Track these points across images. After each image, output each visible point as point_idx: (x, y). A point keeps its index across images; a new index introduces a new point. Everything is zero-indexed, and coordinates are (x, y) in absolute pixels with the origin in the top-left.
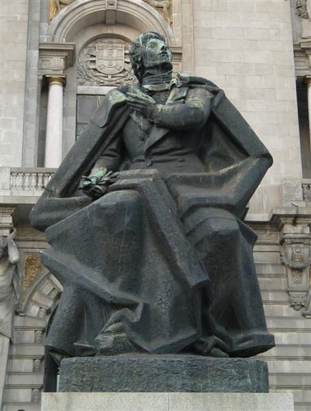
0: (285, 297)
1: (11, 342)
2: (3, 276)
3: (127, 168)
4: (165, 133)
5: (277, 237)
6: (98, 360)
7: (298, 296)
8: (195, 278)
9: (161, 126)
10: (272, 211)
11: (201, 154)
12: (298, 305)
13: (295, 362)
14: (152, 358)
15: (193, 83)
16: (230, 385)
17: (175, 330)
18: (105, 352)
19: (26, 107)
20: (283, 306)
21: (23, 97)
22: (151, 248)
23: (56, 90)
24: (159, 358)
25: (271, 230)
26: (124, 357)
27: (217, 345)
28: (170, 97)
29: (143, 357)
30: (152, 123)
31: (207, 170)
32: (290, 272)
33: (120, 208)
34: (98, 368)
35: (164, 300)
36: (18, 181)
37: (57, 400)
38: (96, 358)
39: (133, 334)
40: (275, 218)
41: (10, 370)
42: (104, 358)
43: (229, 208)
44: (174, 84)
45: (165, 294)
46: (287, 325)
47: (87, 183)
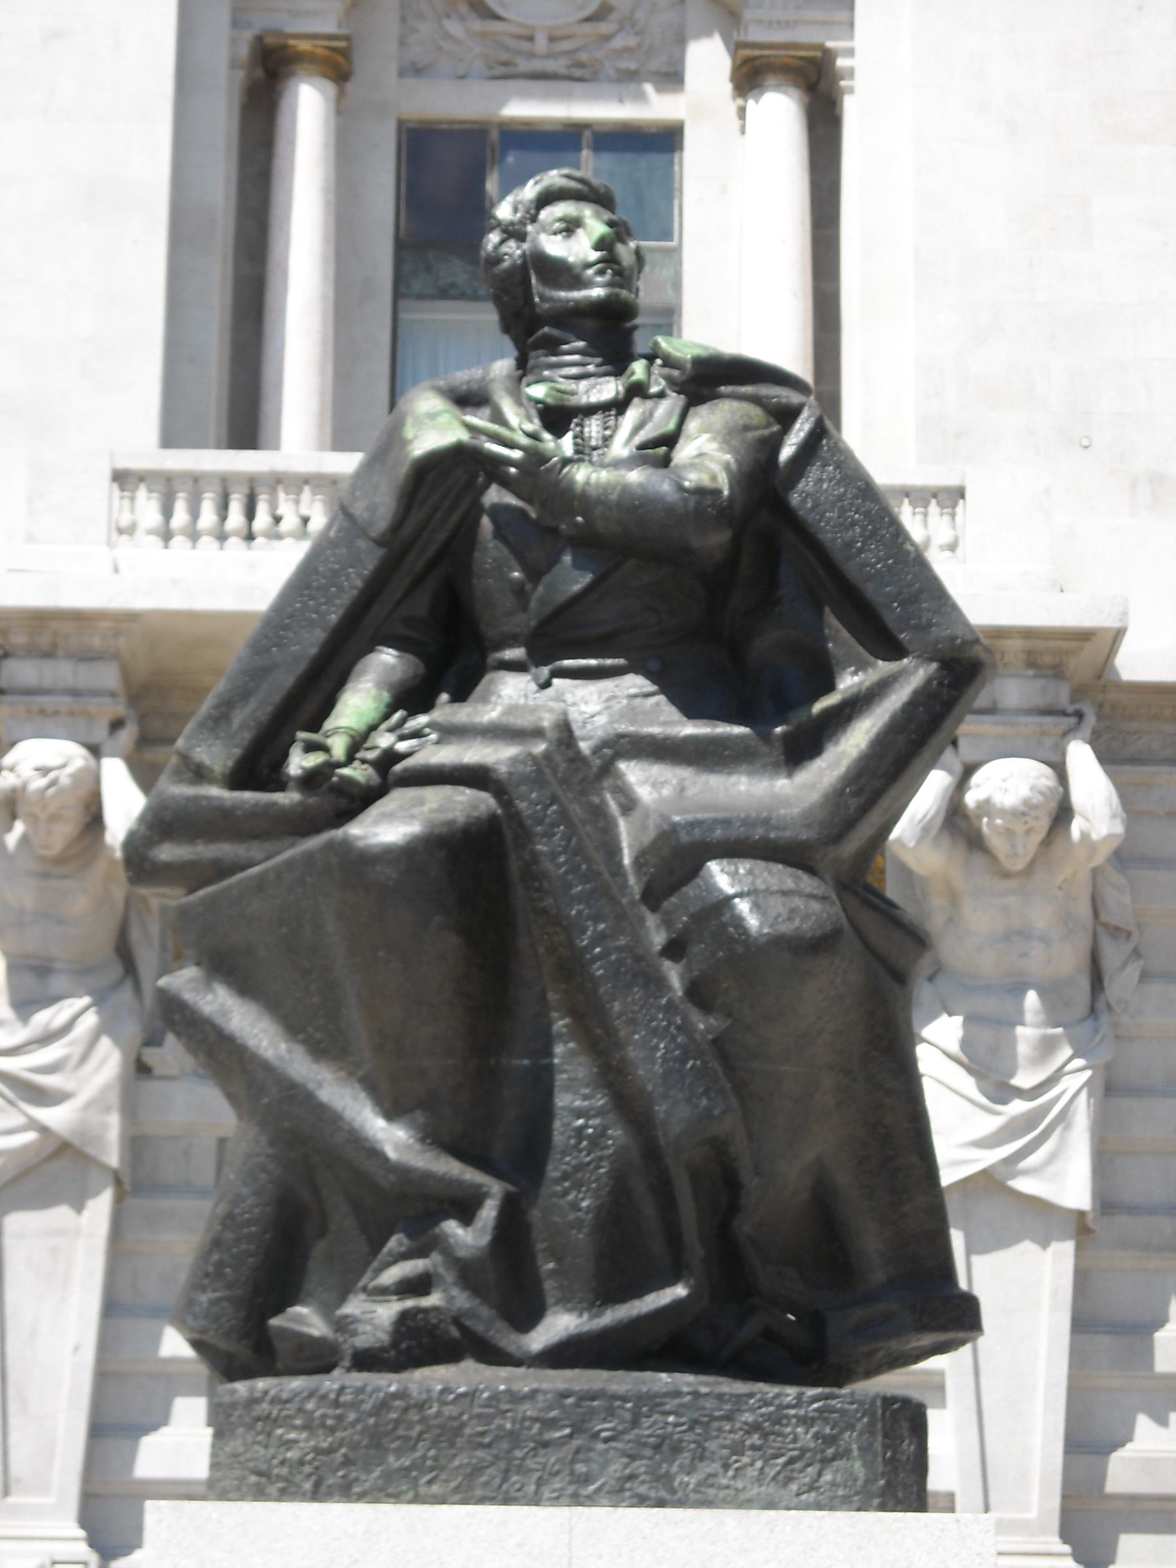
14: (523, 1379)
15: (708, 379)
18: (366, 1361)
23: (309, 106)
38: (329, 1383)
42: (358, 1378)
47: (314, 760)
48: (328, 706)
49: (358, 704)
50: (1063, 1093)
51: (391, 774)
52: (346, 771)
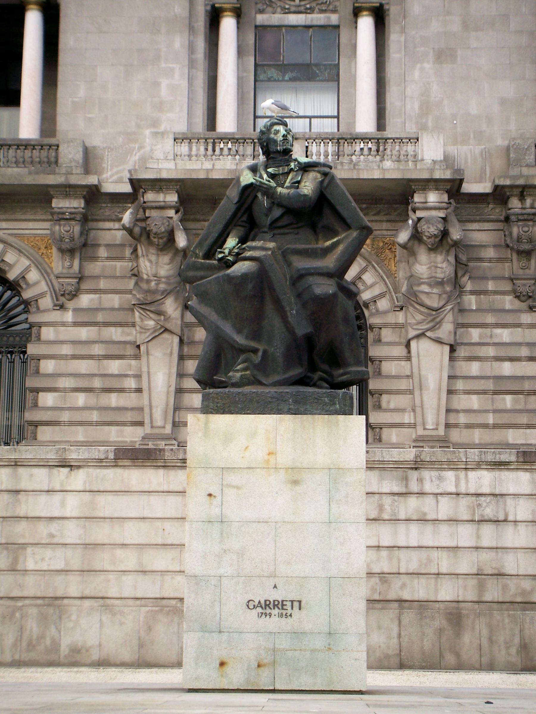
0: (507, 286)
1: (181, 341)
2: (169, 264)
3: (253, 240)
4: (283, 211)
5: (502, 211)
6: (228, 392)
7: (524, 285)
8: (302, 329)
9: (280, 205)
10: (494, 181)
11: (314, 227)
12: (524, 296)
13: (516, 363)
14: (267, 390)
15: (306, 168)
16: (323, 409)
17: (287, 368)
18: (234, 385)
19: (191, 49)
20: (506, 297)
21: (186, 38)
22: (269, 307)
23: (228, 25)
24: (273, 390)
25: (495, 204)
26: (247, 389)
27: (321, 379)
28: (288, 181)
29: (259, 389)
30: (273, 203)
31: (317, 241)
32: (515, 256)
33: (245, 277)
34: (228, 397)
35: (279, 346)
36: (184, 148)
37: (198, 420)
38: (227, 390)
39: (256, 372)
40: (499, 189)
41: (181, 373)
43: (329, 275)
44: (292, 168)
45: (279, 342)
46: (509, 319)
47: (220, 256)
48: (224, 242)
49: (231, 242)
50: (444, 310)
51: (238, 257)
52: (228, 258)
